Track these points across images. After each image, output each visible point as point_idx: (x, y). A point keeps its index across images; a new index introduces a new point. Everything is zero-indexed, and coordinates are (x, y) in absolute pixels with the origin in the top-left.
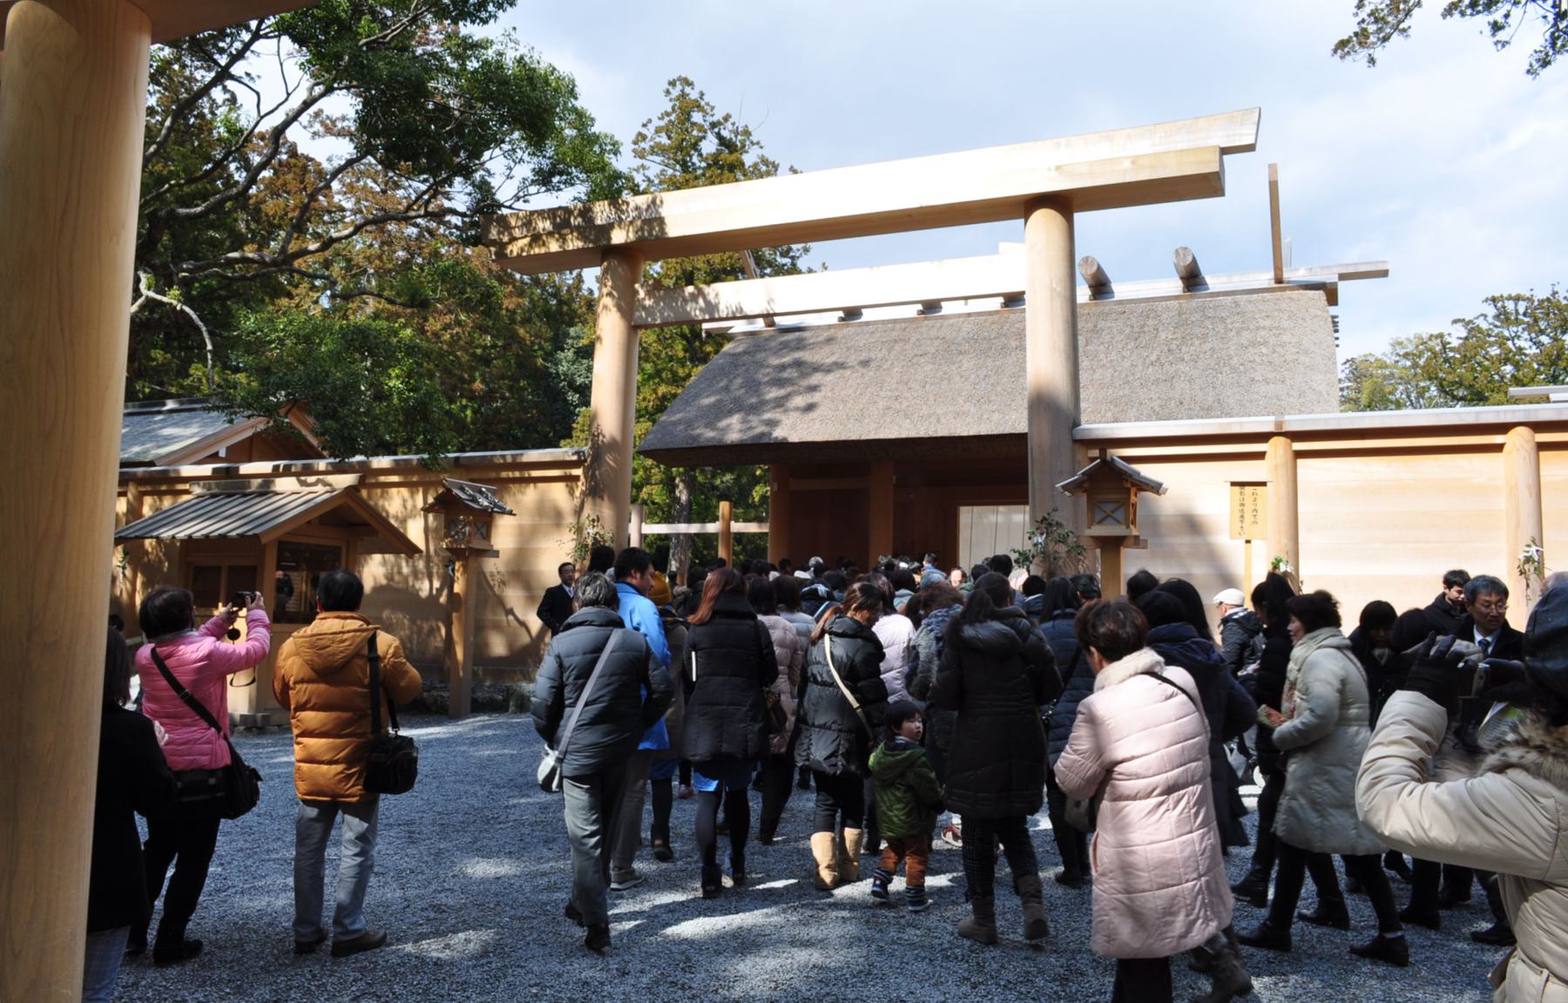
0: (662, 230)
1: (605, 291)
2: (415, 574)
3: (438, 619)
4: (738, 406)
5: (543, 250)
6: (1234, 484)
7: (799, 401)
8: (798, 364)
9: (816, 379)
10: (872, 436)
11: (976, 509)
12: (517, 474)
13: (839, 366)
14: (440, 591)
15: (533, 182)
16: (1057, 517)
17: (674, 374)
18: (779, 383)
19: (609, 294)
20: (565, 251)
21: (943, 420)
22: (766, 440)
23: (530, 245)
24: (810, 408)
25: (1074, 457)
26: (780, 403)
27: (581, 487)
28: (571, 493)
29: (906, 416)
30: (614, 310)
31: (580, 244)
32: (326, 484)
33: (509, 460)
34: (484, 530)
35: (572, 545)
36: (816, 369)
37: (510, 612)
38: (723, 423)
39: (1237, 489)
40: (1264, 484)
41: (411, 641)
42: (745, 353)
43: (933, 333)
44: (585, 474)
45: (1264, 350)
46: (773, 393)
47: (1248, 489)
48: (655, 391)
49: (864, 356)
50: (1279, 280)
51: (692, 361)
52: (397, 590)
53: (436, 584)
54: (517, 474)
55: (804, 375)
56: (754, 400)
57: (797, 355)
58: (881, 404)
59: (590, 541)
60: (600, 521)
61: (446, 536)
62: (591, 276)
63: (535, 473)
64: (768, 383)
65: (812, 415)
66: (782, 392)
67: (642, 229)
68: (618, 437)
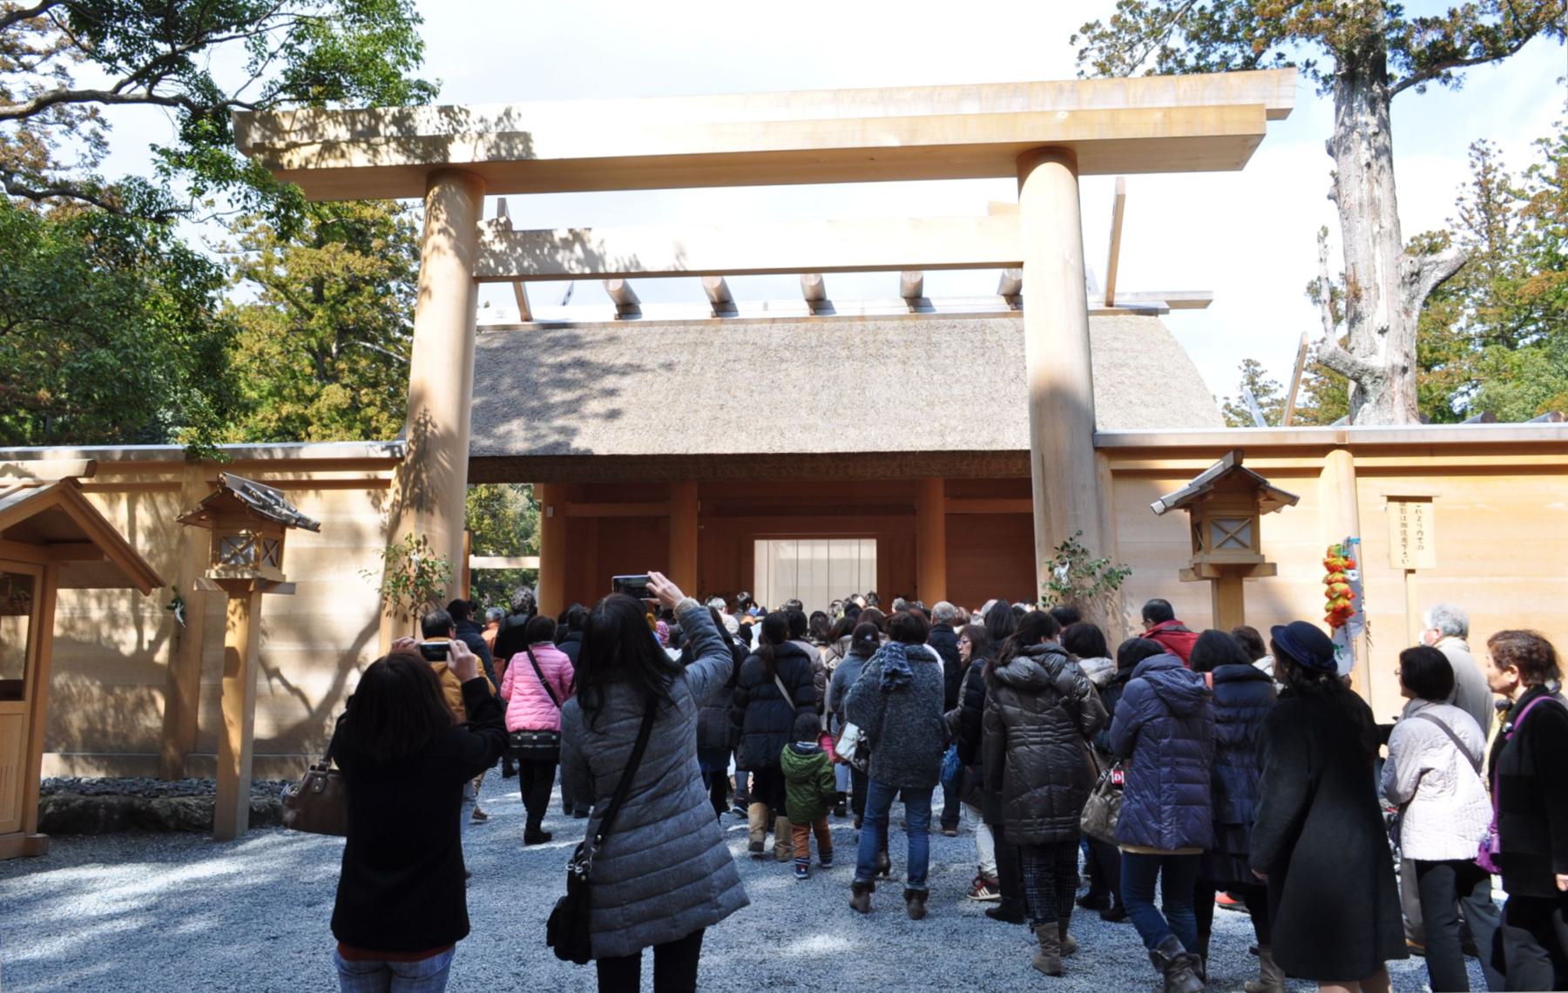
0: (528, 149)
1: (436, 226)
2: (114, 620)
3: (150, 687)
4: (514, 411)
5: (341, 164)
6: (1391, 499)
7: (596, 406)
8: (581, 364)
9: (610, 382)
10: (702, 450)
11: (771, 542)
12: (290, 476)
13: (638, 368)
14: (155, 645)
15: (283, 89)
16: (1082, 542)
17: (300, 392)
18: (567, 385)
19: (442, 231)
20: (376, 167)
21: (788, 435)
22: (563, 452)
23: (320, 154)
24: (613, 415)
25: (1096, 468)
26: (572, 408)
27: (392, 495)
28: (376, 503)
29: (740, 429)
30: (451, 253)
31: (400, 159)
32: (22, 474)
33: (279, 455)
34: (273, 552)
35: (377, 581)
36: (608, 370)
37: (274, 673)
38: (502, 429)
39: (1396, 505)
40: (1428, 499)
41: (103, 720)
42: (504, 348)
43: (739, 337)
44: (399, 475)
45: (1129, 373)
46: (558, 396)
47: (1411, 506)
48: (278, 410)
49: (662, 359)
50: (1110, 304)
51: (319, 378)
52: (80, 644)
53: (150, 634)
54: (290, 476)
55: (594, 378)
56: (535, 403)
57: (576, 354)
58: (705, 414)
59: (412, 572)
60: (433, 542)
61: (216, 560)
62: (413, 211)
63: (318, 476)
64: (547, 384)
65: (617, 423)
66: (570, 396)
67: (497, 146)
68: (454, 426)
